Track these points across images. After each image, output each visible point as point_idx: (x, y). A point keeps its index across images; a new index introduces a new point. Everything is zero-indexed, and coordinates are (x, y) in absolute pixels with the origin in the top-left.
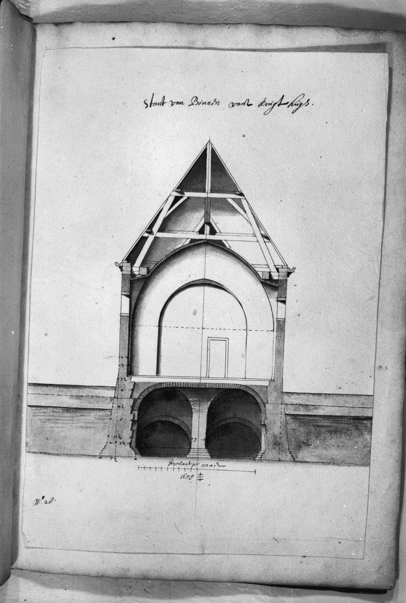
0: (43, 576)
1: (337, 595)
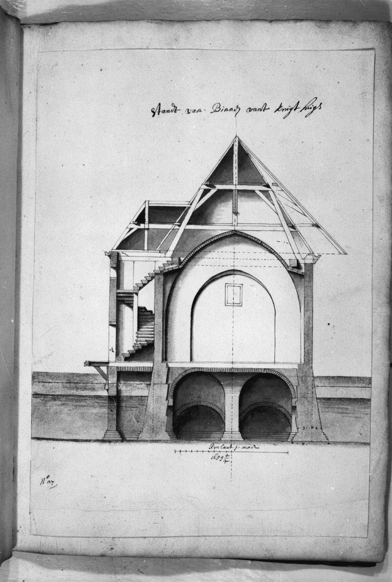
0: (41, 555)
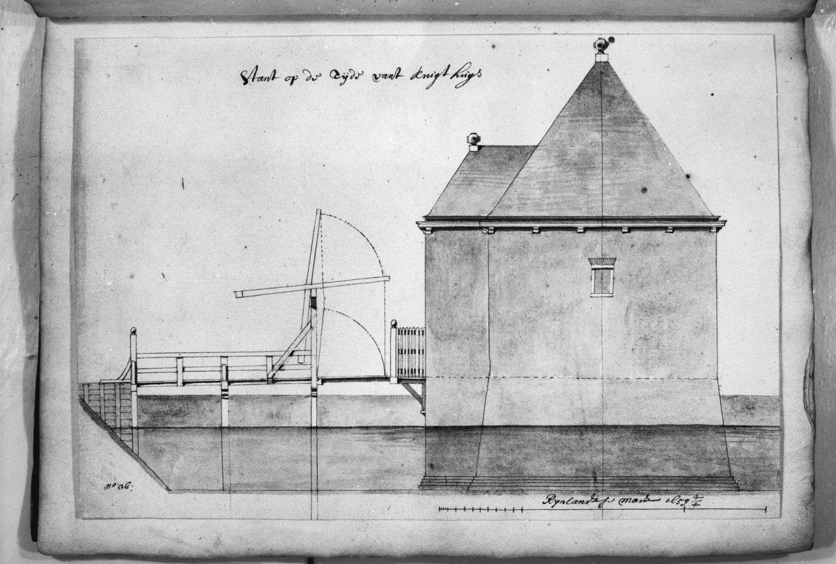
0: (41, 56)
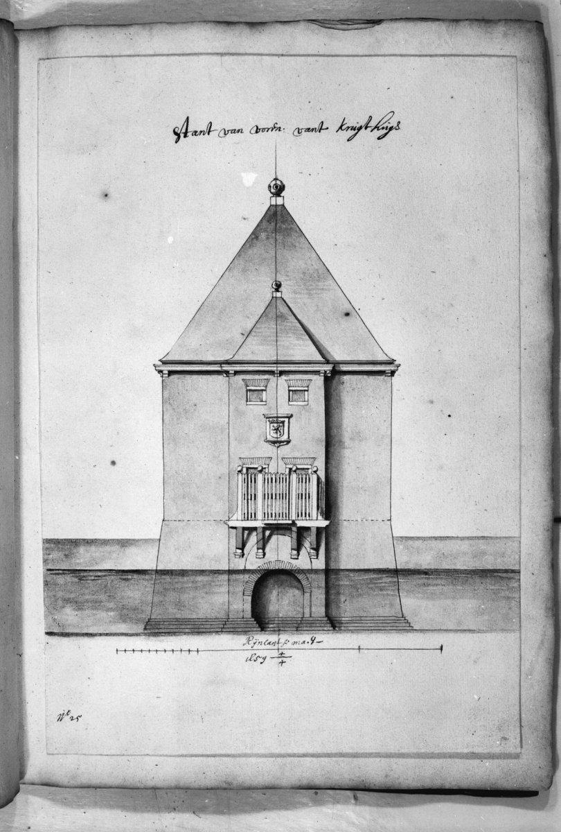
1: (439, 801)
